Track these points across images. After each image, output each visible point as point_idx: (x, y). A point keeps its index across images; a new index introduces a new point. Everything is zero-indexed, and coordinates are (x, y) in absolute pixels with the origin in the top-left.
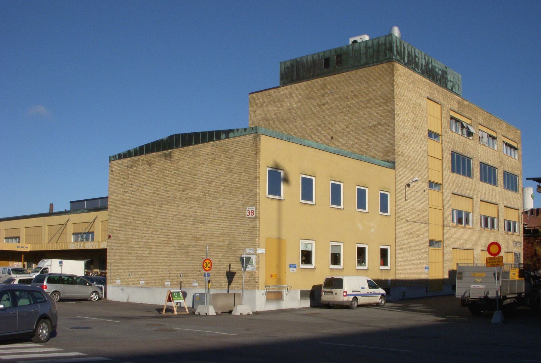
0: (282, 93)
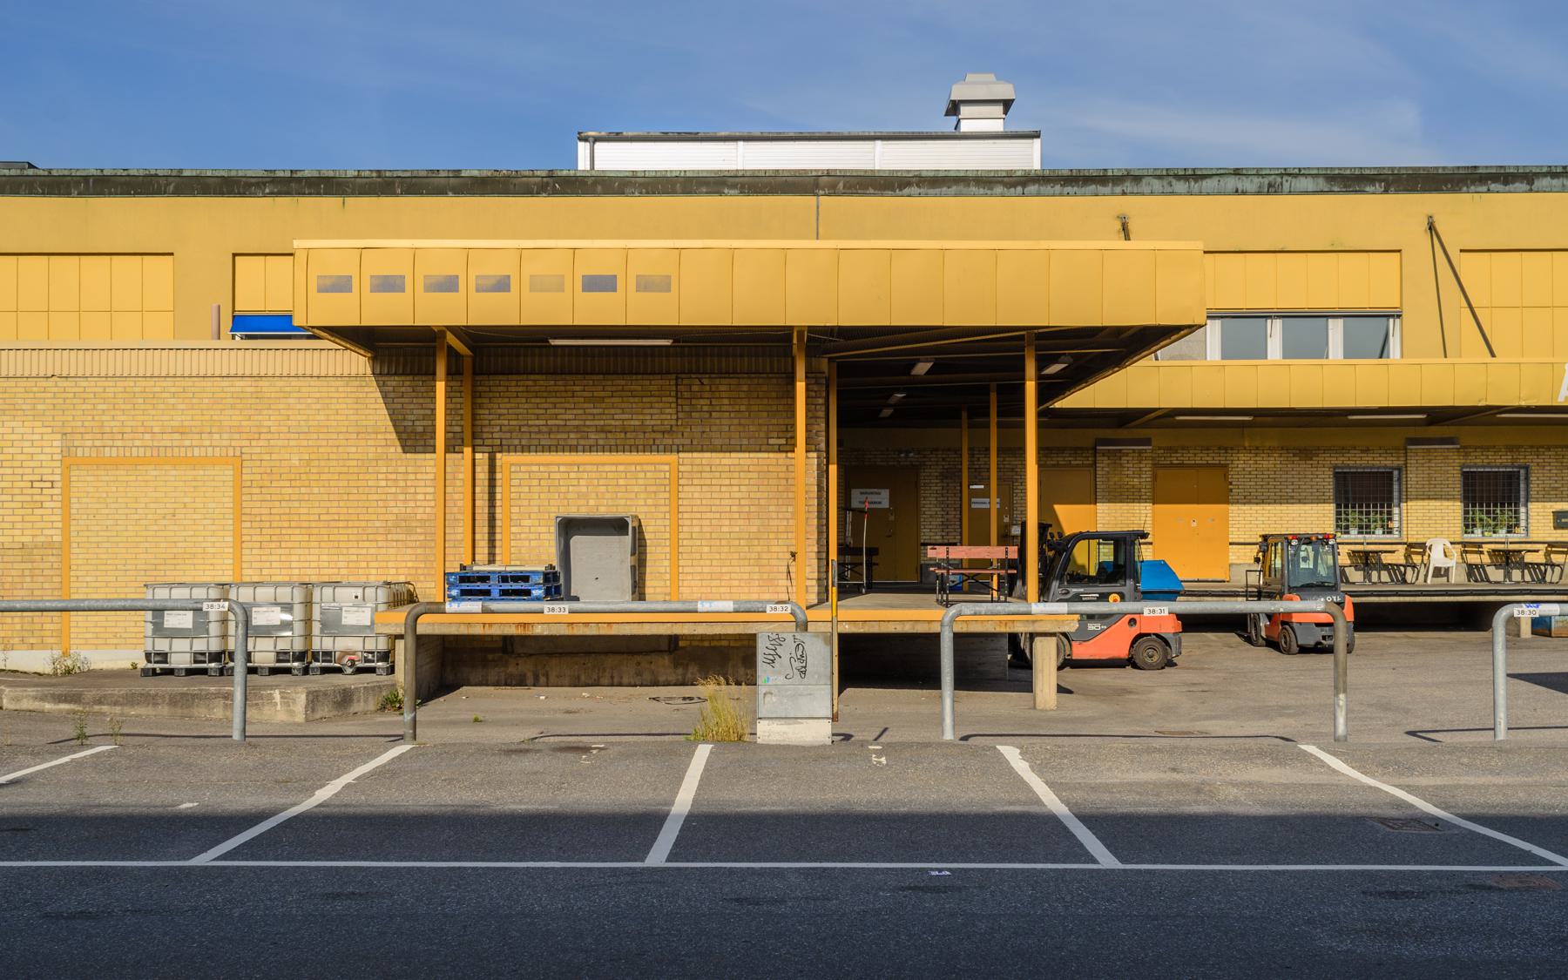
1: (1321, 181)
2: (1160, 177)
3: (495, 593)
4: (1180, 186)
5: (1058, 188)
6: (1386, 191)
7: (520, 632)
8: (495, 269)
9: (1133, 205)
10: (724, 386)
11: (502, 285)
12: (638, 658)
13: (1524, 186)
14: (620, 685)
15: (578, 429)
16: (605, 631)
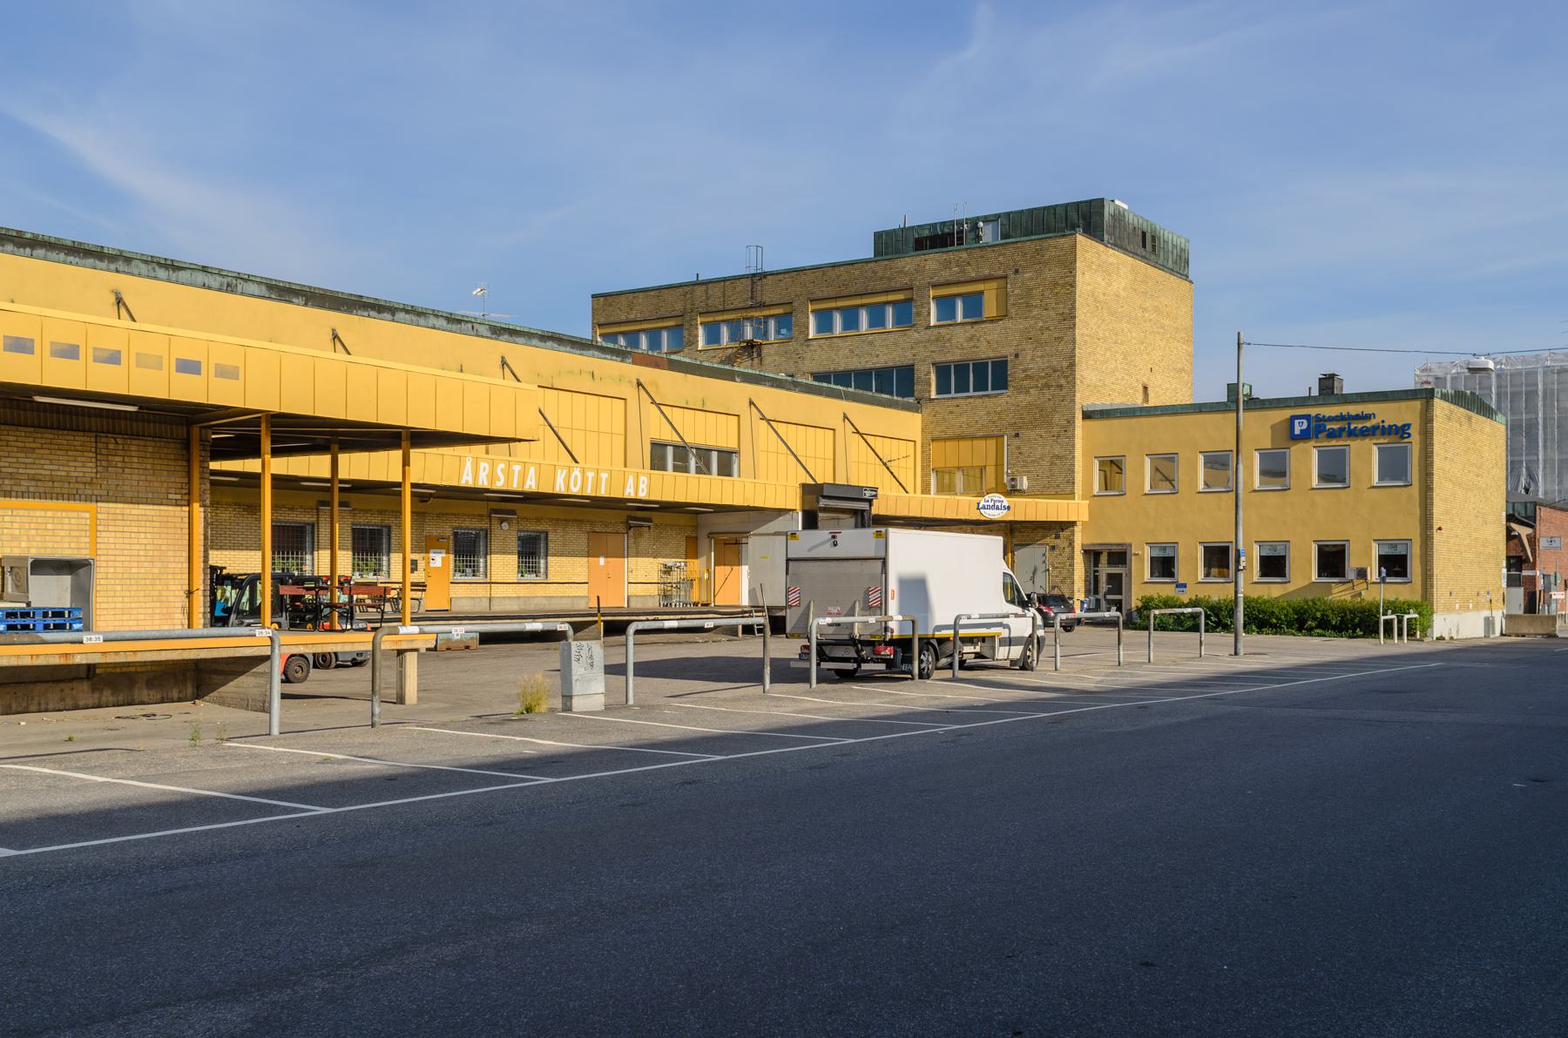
0: (1112, 260)
1: (263, 288)
2: (146, 262)
3: (40, 626)
4: (161, 273)
5: (62, 256)
6: (306, 305)
7: (62, 661)
8: (110, 343)
9: (133, 286)
10: (134, 446)
11: (114, 358)
12: (62, 685)
13: (389, 316)
14: (46, 710)
15: (11, 476)
16: (131, 658)
